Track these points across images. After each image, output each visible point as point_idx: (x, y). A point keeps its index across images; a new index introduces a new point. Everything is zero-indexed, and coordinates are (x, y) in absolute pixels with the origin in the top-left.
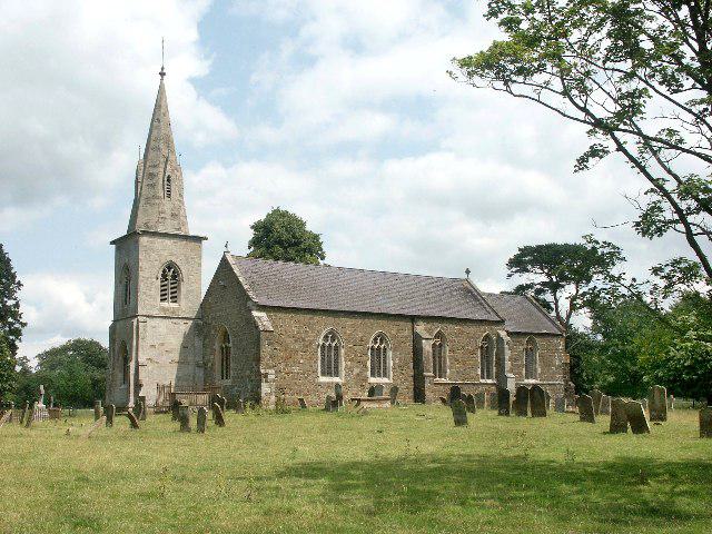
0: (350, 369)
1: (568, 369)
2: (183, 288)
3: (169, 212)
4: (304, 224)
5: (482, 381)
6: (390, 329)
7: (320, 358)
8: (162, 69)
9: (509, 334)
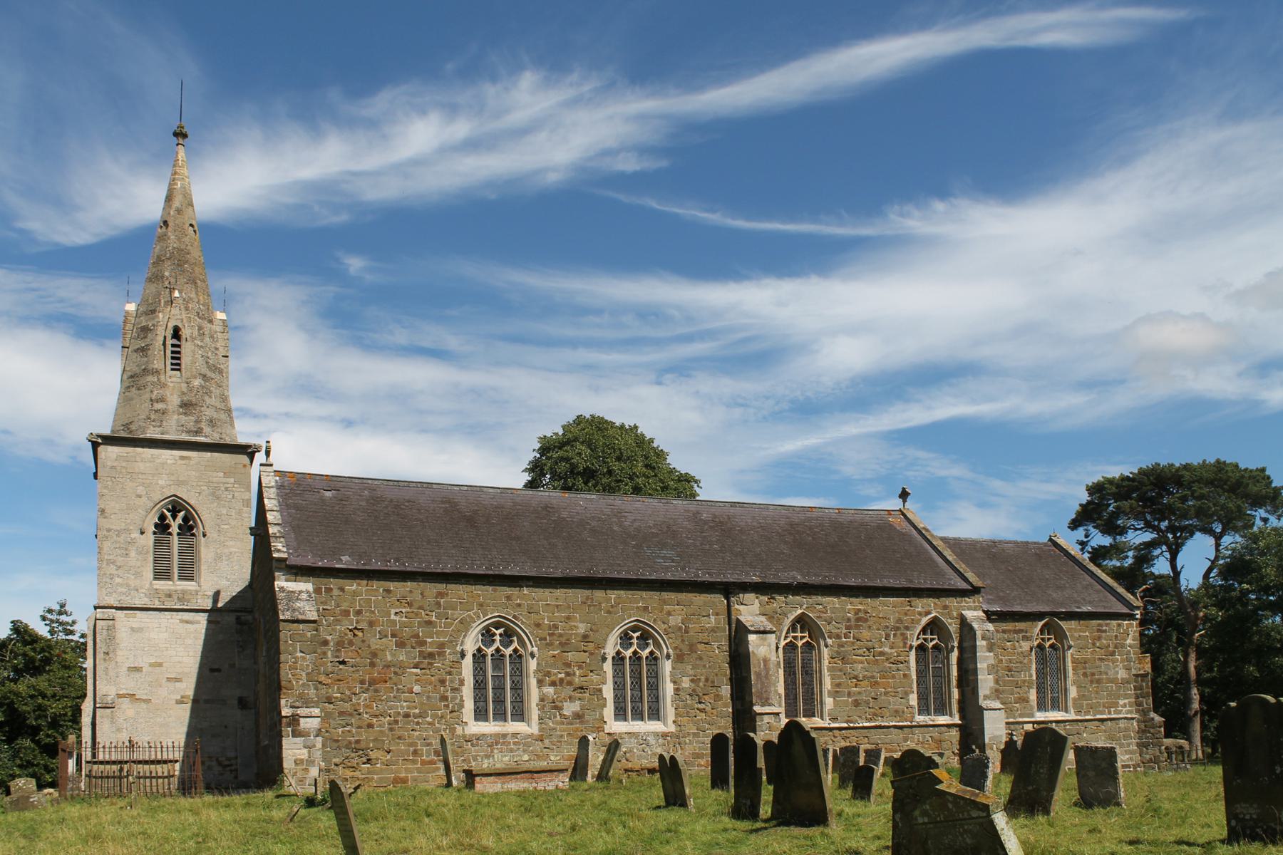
0: (551, 706)
1: (1147, 686)
3: (174, 400)
5: (921, 719)
6: (671, 612)
9: (990, 616)
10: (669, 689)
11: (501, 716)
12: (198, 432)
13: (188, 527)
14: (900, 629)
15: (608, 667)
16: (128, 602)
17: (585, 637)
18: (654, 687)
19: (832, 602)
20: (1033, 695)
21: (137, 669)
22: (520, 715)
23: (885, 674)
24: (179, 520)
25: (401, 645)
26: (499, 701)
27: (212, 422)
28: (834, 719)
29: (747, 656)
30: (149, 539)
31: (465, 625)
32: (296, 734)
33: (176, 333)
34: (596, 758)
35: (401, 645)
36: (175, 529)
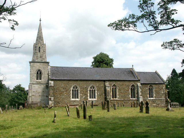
0: (81, 97)
2: (43, 76)
4: (108, 56)
5: (131, 99)
6: (98, 84)
7: (71, 93)
8: (40, 19)
9: (141, 84)
10: (96, 94)
11: (75, 98)
12: (42, 60)
13: (40, 73)
14: (128, 86)
15: (89, 92)
16: (33, 83)
17: (86, 87)
18: (95, 94)
19: (119, 82)
20: (148, 96)
21: (34, 92)
22: (78, 98)
23: (126, 92)
24: (40, 72)
25: (63, 89)
26: (75, 96)
27: (44, 59)
28: (119, 99)
29: (106, 90)
30: (36, 75)
31: (71, 86)
32: (51, 100)
33: (40, 48)
34: (144, 109)
35: (63, 89)
36: (39, 73)
